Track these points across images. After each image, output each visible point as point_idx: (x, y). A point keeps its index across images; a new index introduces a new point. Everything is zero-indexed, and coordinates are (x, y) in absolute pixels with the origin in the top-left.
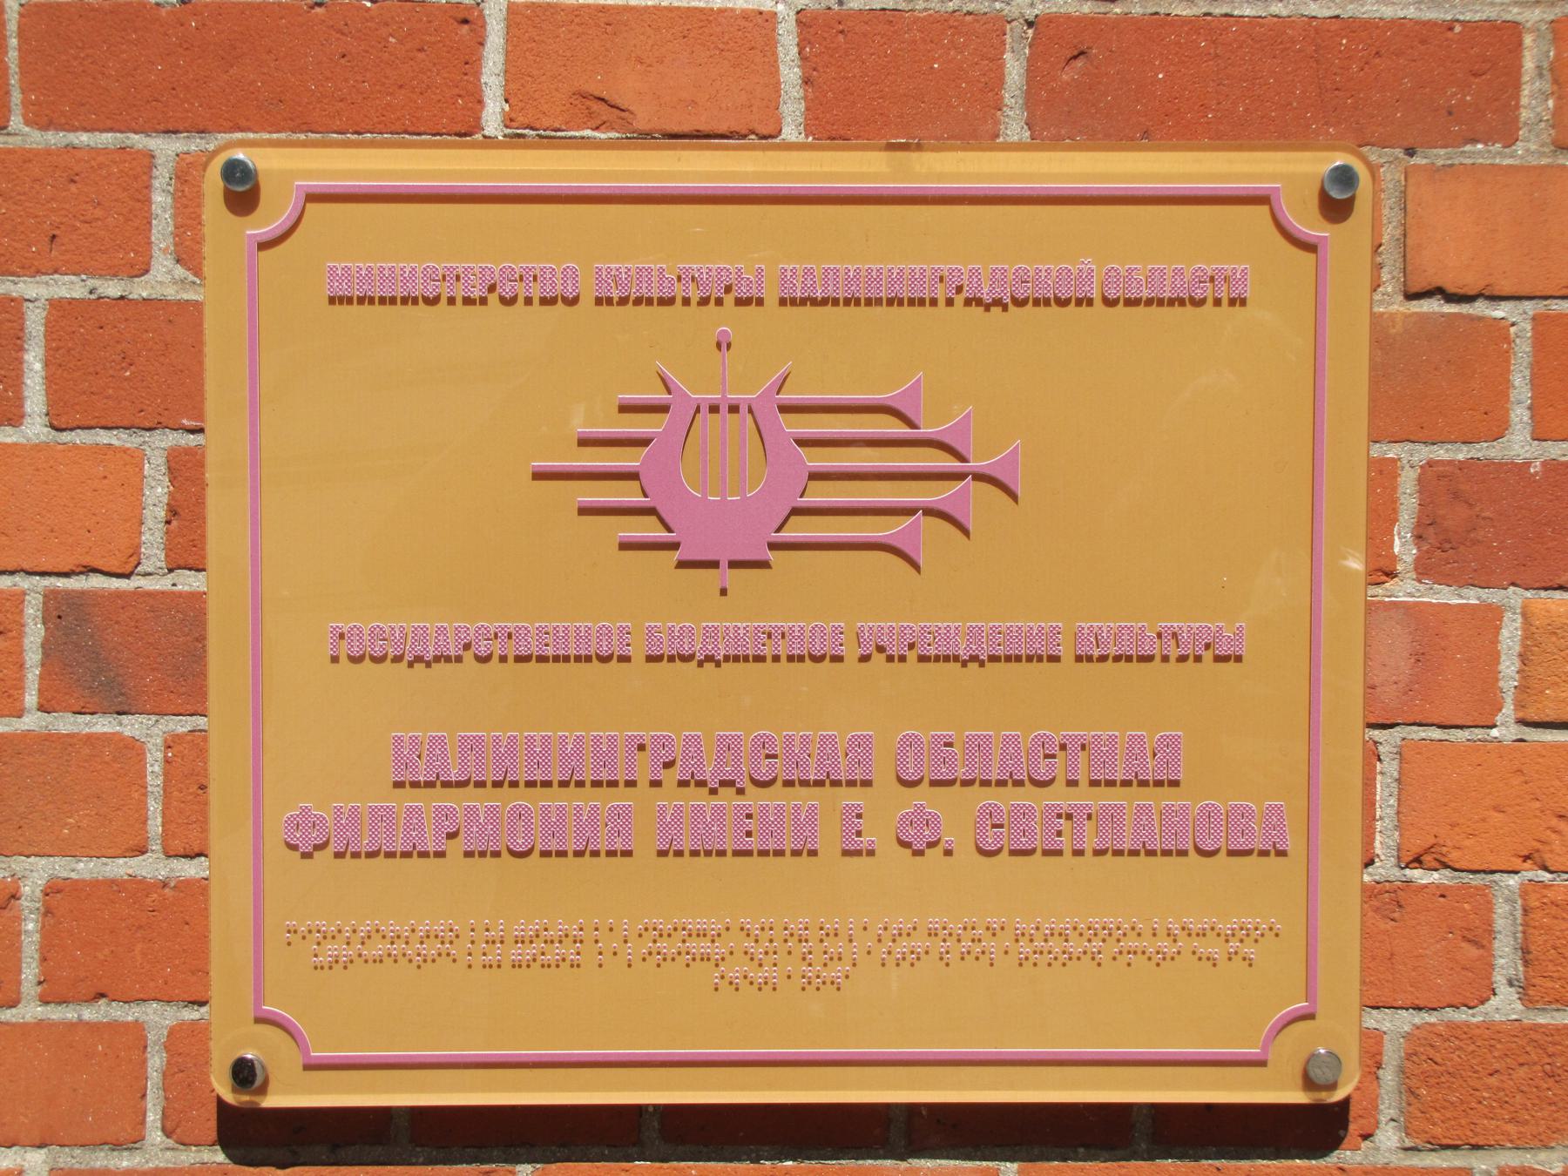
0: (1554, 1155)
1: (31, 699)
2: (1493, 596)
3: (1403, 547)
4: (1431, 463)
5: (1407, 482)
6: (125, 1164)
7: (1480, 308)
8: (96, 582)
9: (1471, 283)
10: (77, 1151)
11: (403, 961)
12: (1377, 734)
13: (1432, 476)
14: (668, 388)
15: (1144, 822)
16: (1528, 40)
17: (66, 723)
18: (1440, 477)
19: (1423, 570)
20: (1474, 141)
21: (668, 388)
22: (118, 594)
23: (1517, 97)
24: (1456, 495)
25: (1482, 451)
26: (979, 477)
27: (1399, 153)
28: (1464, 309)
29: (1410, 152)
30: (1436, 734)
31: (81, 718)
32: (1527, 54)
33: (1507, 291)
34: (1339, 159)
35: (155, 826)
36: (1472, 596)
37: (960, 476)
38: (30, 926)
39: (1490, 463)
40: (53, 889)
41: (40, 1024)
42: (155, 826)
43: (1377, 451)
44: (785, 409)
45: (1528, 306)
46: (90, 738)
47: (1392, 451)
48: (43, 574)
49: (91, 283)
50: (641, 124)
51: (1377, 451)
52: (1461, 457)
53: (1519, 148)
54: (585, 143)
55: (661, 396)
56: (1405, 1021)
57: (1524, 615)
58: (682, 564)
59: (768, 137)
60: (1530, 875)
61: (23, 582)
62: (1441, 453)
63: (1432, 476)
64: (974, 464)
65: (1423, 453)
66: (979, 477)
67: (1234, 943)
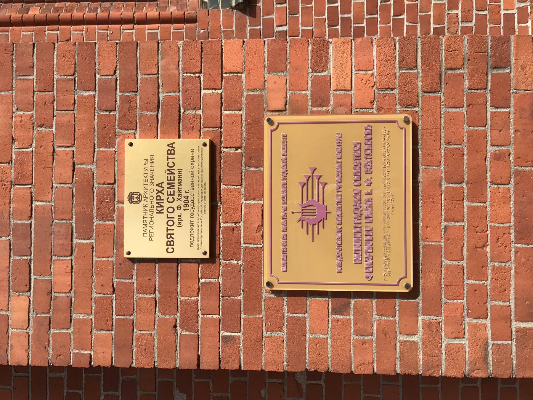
0: (419, 84)
1: (348, 317)
2: (332, 95)
3: (324, 109)
4: (311, 105)
5: (314, 109)
6: (421, 304)
7: (288, 99)
8: (330, 306)
9: (284, 100)
10: (419, 312)
11: (389, 263)
12: (353, 112)
13: (313, 106)
14: (300, 220)
15: (170, 247)
16: (248, 93)
17: (352, 312)
18: (313, 104)
19: (328, 106)
20: (263, 101)
21: (300, 220)
22: (332, 304)
23: (257, 95)
24: (316, 101)
25: (309, 98)
26: (313, 173)
27: (265, 112)
28: (288, 101)
29: (265, 110)
30: (353, 103)
31: (351, 310)
32: (250, 94)
33: (285, 95)
34: (265, 121)
35: (357, 382)
36: (332, 98)
37: (313, 175)
38: (384, 318)
39: (311, 97)
40: (378, 314)
41: (399, 317)
42: (357, 382)
43: (309, 114)
44: (302, 203)
45: (288, 91)
46: (354, 308)
47: (309, 111)
48: (329, 315)
49: (285, 306)
50: (260, 224)
51: (309, 114)
52: (310, 101)
53: (264, 94)
54: (263, 232)
55: (301, 222)
56: (398, 106)
57: (334, 90)
58: (327, 219)
59: (263, 205)
60: (375, 88)
61: (330, 317)
62: (310, 104)
63: (313, 106)
64: (311, 174)
65: (310, 106)
66: (313, 173)
67: (386, 134)
